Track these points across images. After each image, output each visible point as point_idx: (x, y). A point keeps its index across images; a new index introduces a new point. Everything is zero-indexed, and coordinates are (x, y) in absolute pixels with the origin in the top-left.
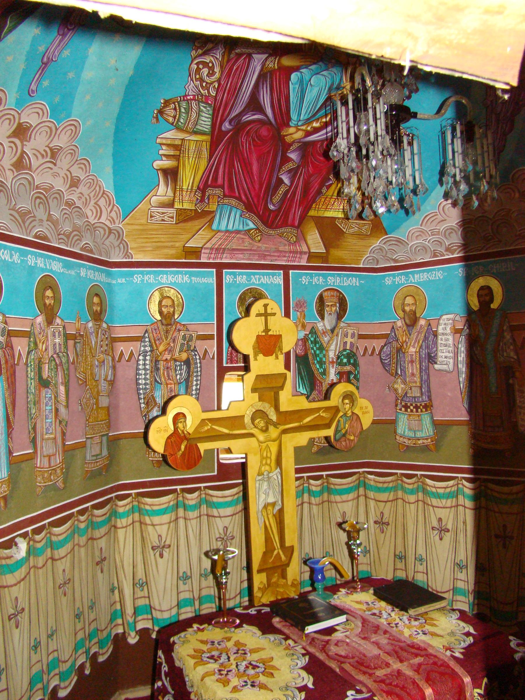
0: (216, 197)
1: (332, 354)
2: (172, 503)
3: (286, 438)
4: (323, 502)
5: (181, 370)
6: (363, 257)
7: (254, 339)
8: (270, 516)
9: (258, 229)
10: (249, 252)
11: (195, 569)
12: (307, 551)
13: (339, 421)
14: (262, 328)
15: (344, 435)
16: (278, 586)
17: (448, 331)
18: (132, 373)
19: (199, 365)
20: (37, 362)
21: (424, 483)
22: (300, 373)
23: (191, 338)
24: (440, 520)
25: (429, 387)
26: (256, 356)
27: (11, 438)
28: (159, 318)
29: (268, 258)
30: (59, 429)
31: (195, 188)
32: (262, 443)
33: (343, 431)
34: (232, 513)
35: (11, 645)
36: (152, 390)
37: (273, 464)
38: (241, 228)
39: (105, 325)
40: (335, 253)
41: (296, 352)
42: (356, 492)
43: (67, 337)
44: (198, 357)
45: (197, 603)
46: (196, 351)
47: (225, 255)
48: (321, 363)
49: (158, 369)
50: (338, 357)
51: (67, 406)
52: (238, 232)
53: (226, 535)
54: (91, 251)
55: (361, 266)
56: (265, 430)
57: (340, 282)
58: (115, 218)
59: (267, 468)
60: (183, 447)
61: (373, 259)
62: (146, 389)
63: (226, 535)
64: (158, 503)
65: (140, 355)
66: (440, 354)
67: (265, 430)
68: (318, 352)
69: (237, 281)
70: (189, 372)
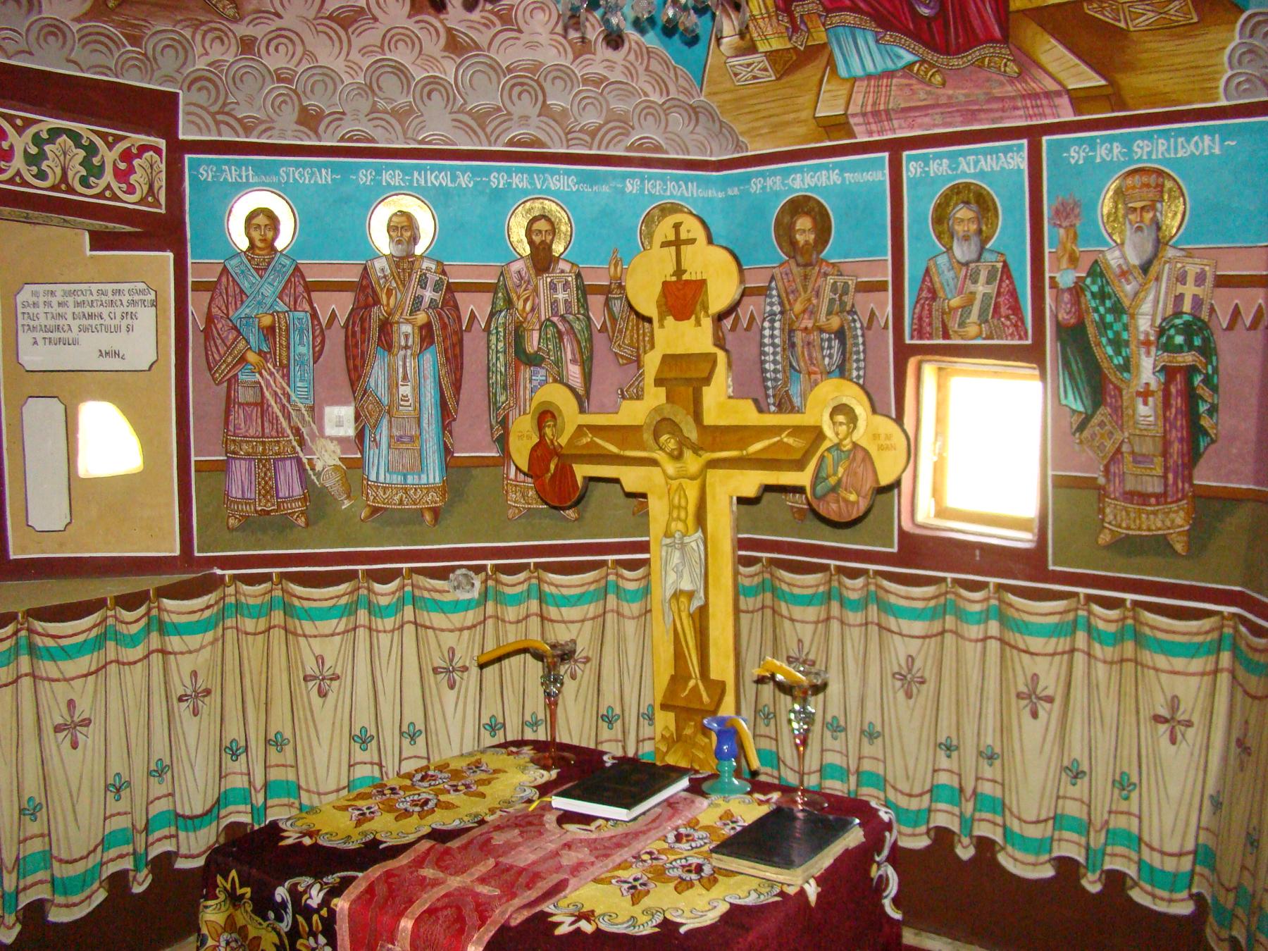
0: (814, 17)
1: (1144, 324)
2: (821, 589)
3: (714, 476)
4: (1122, 661)
5: (830, 347)
6: (1218, 80)
7: (659, 288)
8: (684, 615)
9: (923, 61)
10: (939, 110)
11: (853, 719)
12: (1076, 754)
13: (822, 458)
14: (671, 267)
15: (834, 489)
16: (694, 745)
19: (860, 340)
20: (512, 328)
22: (1066, 365)
23: (845, 291)
26: (661, 320)
27: (450, 432)
29: (982, 116)
31: (772, 9)
32: (672, 478)
33: (832, 481)
34: (922, 634)
35: (437, 706)
36: (785, 384)
37: (691, 520)
38: (891, 66)
40: (1132, 82)
41: (1056, 317)
42: (1212, 659)
43: (584, 291)
44: (858, 325)
45: (853, 779)
46: (855, 313)
47: (896, 123)
48: (1117, 344)
49: (793, 345)
50: (1161, 332)
52: (889, 74)
53: (910, 670)
54: (658, 148)
55: (1223, 103)
56: (677, 457)
57: (1168, 150)
58: (687, 86)
59: (680, 526)
60: (552, 467)
61: (1247, 81)
62: (776, 380)
63: (910, 670)
64: (1165, 627)
65: (764, 320)
67: (677, 457)
68: (1109, 318)
69: (930, 171)
70: (844, 353)
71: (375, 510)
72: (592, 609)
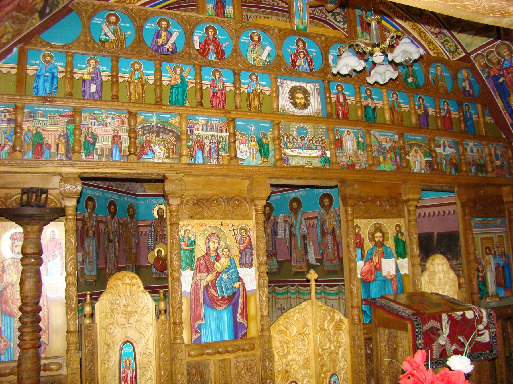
17: (282, 221)
18: (146, 240)
21: (275, 289)
24: (281, 305)
25: (275, 246)
28: (157, 217)
30: (115, 260)
39: (135, 220)
43: (119, 224)
49: (157, 238)
51: (119, 251)
54: (129, 190)
66: (279, 231)
71: (86, 281)
72: (338, 297)
